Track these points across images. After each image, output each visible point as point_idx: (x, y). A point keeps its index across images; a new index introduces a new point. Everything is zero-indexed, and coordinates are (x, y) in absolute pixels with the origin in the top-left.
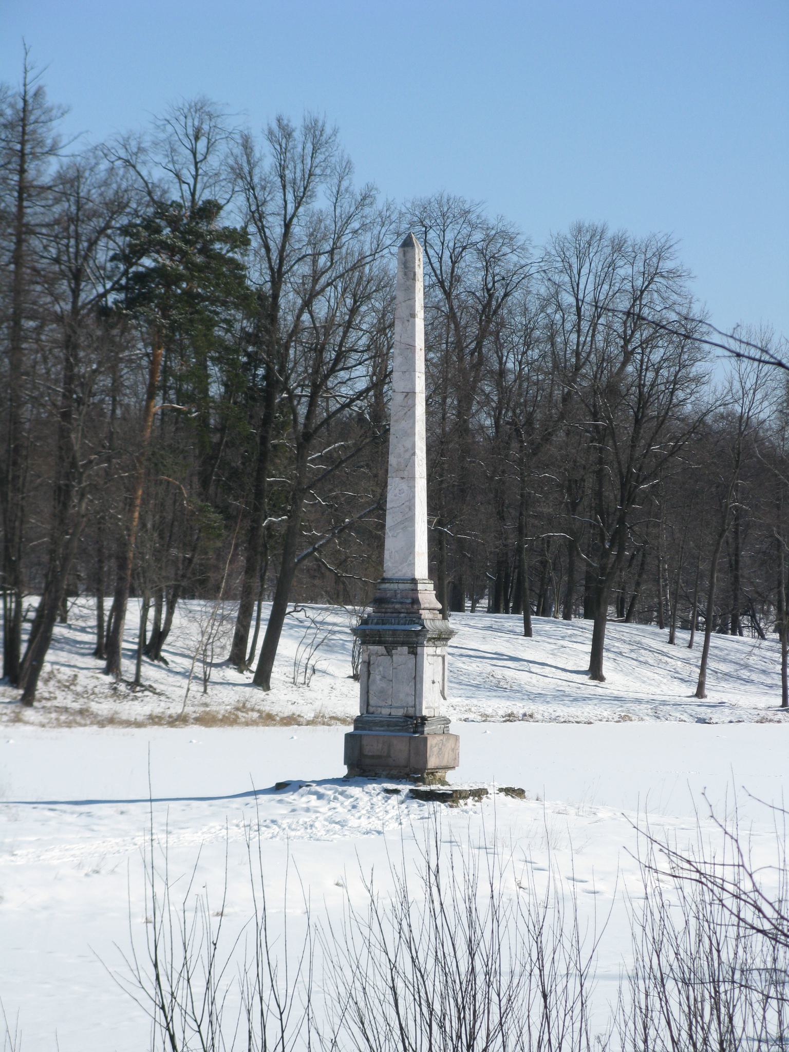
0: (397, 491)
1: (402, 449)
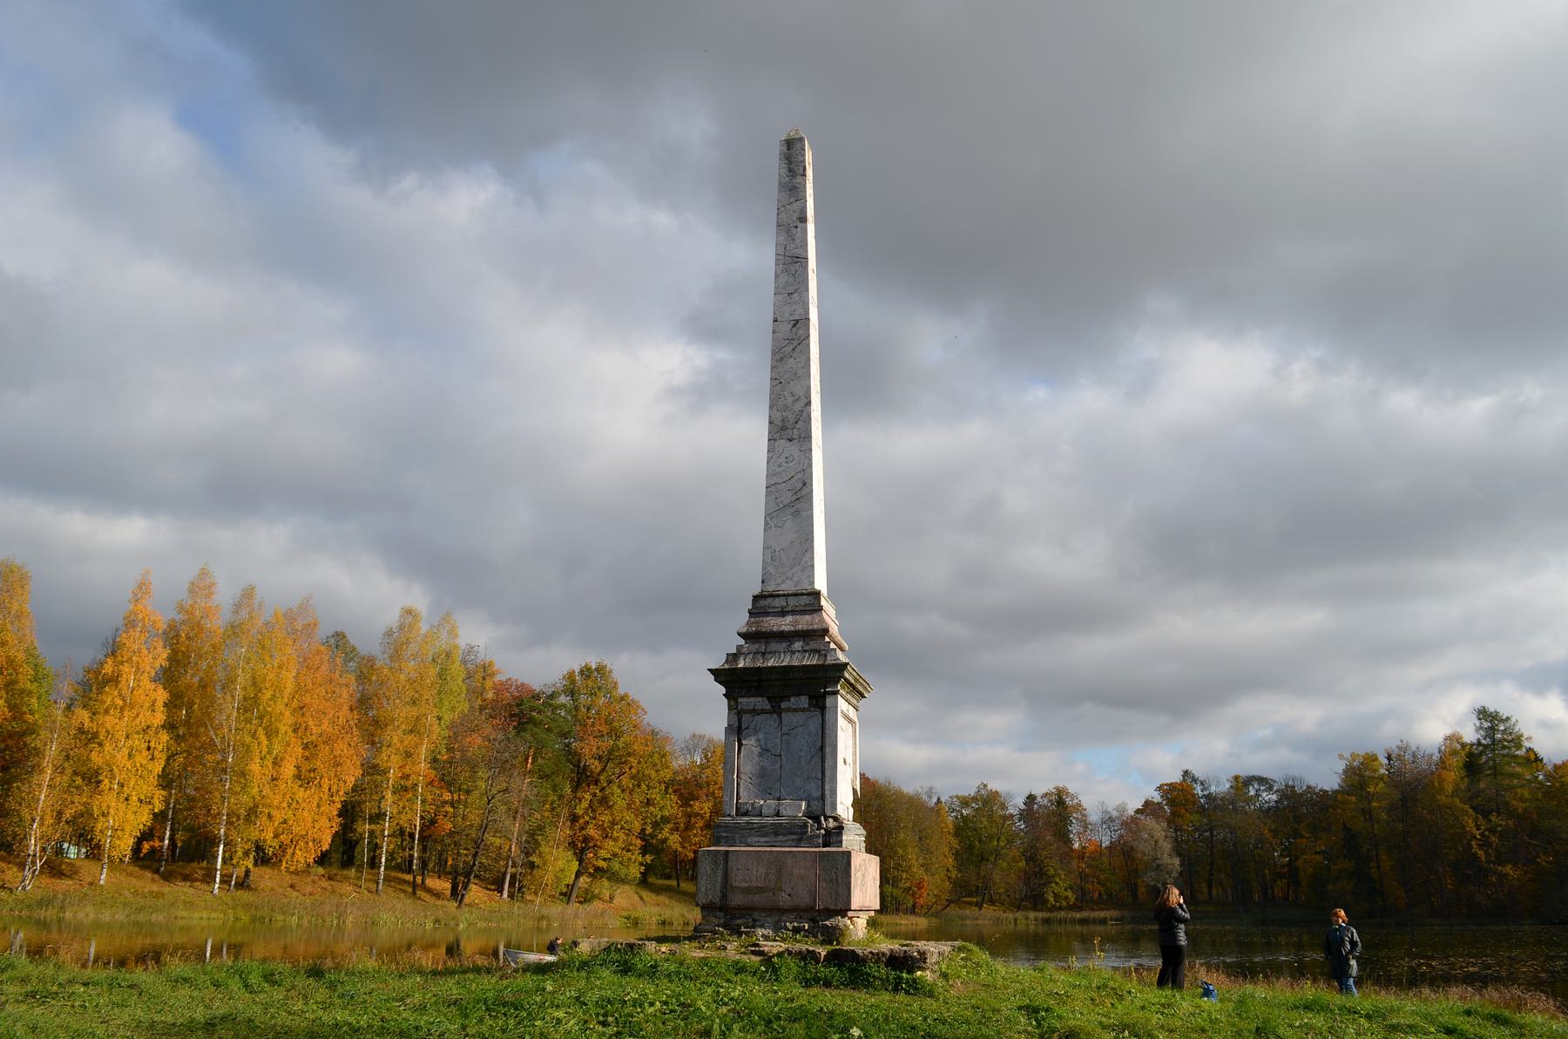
0: (783, 459)
1: (790, 399)
